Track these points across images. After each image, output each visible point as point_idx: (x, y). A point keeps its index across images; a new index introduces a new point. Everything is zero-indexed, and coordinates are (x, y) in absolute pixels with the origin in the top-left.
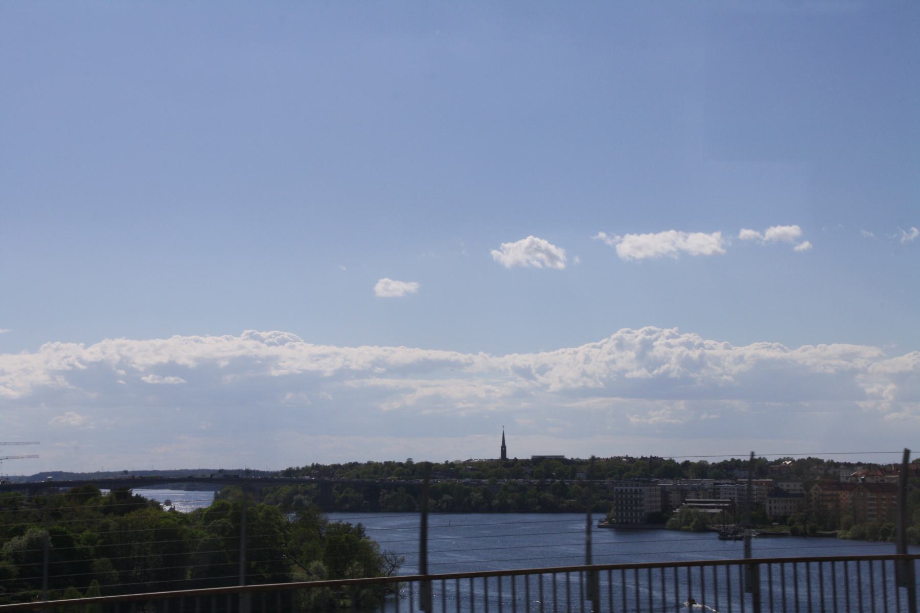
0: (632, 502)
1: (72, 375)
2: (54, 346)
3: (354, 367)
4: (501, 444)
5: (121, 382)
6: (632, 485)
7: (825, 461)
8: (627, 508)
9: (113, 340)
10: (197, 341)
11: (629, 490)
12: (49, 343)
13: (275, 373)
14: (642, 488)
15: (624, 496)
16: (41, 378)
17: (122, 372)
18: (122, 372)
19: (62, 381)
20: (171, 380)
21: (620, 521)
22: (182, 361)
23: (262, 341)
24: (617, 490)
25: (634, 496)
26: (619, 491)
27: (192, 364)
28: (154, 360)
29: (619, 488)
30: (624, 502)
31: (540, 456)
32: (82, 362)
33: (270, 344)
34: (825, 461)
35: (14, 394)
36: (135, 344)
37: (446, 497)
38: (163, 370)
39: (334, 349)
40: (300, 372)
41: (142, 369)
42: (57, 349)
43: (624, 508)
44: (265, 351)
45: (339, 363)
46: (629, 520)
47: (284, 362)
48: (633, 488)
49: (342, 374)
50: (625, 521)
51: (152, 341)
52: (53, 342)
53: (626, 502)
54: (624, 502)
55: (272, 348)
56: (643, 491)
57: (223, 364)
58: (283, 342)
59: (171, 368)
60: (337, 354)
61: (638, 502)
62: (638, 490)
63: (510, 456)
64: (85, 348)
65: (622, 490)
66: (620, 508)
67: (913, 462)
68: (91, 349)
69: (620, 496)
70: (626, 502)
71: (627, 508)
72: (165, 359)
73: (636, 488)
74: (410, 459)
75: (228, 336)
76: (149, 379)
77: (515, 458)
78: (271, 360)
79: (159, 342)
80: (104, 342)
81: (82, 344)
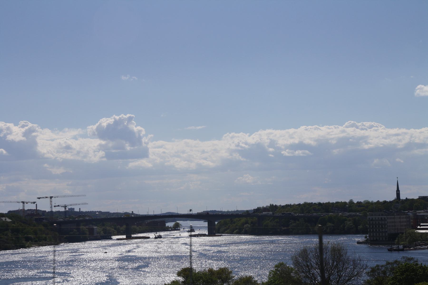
0: (379, 226)
1: (243, 152)
2: (231, 135)
3: (417, 141)
4: (396, 189)
5: (271, 155)
6: (379, 215)
7: (47, 211)
8: (376, 230)
9: (265, 130)
10: (315, 129)
11: (380, 219)
12: (228, 133)
13: (366, 147)
14: (386, 217)
15: (374, 222)
16: (225, 154)
17: (271, 150)
18: (271, 150)
19: (237, 156)
20: (299, 153)
21: (372, 239)
22: (307, 141)
23: (357, 127)
24: (369, 218)
25: (380, 222)
26: (371, 219)
27: (313, 143)
28: (290, 141)
29: (371, 217)
30: (374, 226)
31: (423, 197)
32: (246, 144)
33: (362, 129)
34: (47, 211)
35: (211, 164)
36: (278, 132)
37: (329, 224)
38: (294, 147)
39: (404, 130)
40: (382, 146)
41: (283, 147)
42: (232, 137)
43: (375, 230)
44: (359, 133)
45: (406, 140)
46: (378, 238)
47: (372, 140)
48: (380, 217)
49: (409, 146)
50: (375, 239)
51: (287, 130)
52: (230, 133)
53: (376, 227)
54: (374, 226)
55: (363, 132)
56: (386, 218)
57: (334, 142)
58: (371, 127)
59: (301, 146)
60: (406, 133)
61: (383, 226)
62: (383, 219)
63: (403, 197)
64: (249, 136)
65: (381, 218)
66: (372, 230)
67: (81, 211)
68: (253, 136)
69: (371, 223)
70: (376, 227)
71: (376, 230)
72: (297, 141)
73: (382, 217)
74: (352, 200)
75: (336, 126)
76: (286, 153)
77: (329, 202)
78: (364, 139)
79: (291, 131)
80: (260, 132)
81: (248, 134)
